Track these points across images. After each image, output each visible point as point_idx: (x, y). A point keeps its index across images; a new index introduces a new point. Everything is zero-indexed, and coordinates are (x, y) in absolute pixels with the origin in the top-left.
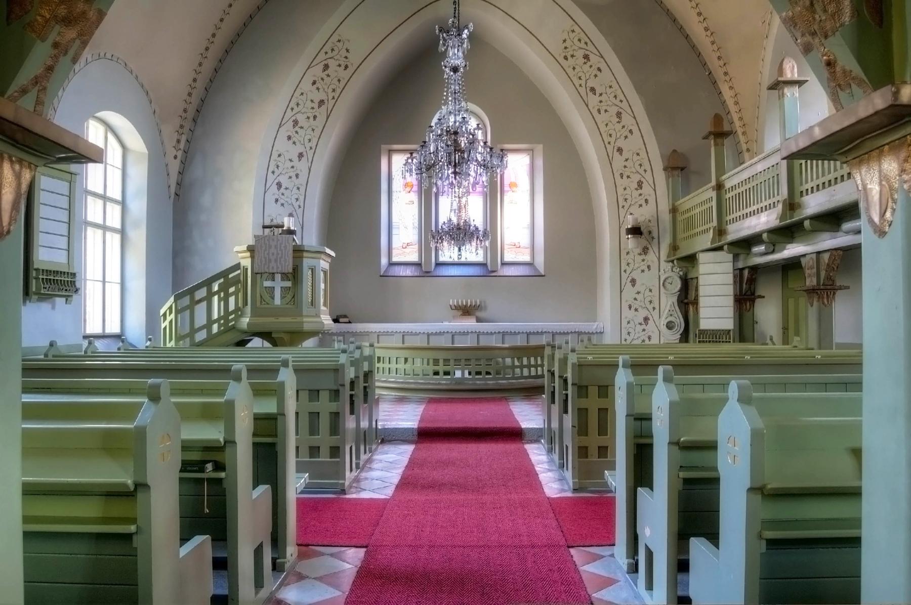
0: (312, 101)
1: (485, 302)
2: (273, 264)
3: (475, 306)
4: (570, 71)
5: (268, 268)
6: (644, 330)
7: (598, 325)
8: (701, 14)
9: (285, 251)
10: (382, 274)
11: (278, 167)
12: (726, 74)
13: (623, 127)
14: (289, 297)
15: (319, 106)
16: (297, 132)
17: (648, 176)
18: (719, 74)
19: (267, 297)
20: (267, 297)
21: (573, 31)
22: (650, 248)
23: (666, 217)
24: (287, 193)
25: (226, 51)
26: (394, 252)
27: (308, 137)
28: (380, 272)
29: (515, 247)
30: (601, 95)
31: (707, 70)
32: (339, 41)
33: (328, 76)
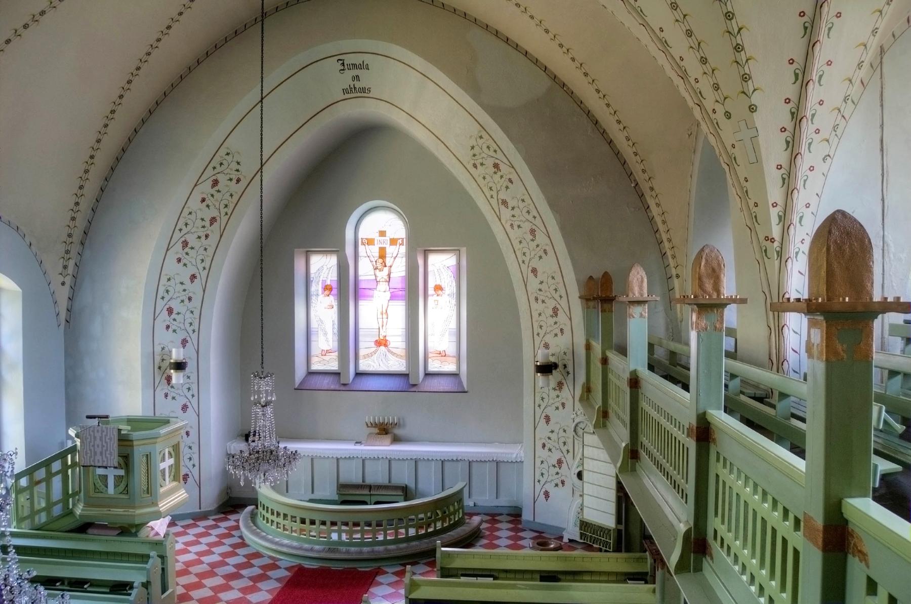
0: (203, 219)
1: (403, 419)
2: (98, 457)
3: (392, 423)
4: (480, 180)
5: (94, 461)
6: (557, 473)
7: (517, 454)
8: (620, 122)
9: (110, 444)
10: (296, 387)
11: (167, 291)
12: (652, 189)
13: (538, 246)
14: (122, 486)
15: (211, 224)
16: (187, 254)
17: (564, 302)
18: (645, 187)
19: (100, 484)
20: (100, 484)
21: (481, 137)
22: (565, 384)
23: (581, 351)
24: (179, 318)
25: (112, 168)
26: (314, 360)
27: (201, 257)
28: (295, 385)
29: (440, 355)
30: (513, 208)
31: (633, 182)
32: (228, 154)
33: (219, 191)
